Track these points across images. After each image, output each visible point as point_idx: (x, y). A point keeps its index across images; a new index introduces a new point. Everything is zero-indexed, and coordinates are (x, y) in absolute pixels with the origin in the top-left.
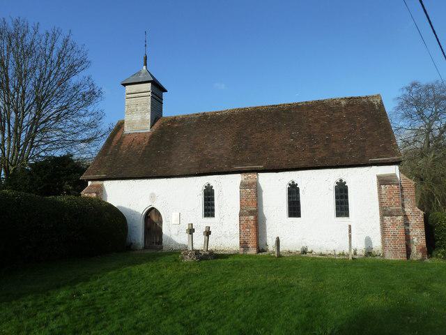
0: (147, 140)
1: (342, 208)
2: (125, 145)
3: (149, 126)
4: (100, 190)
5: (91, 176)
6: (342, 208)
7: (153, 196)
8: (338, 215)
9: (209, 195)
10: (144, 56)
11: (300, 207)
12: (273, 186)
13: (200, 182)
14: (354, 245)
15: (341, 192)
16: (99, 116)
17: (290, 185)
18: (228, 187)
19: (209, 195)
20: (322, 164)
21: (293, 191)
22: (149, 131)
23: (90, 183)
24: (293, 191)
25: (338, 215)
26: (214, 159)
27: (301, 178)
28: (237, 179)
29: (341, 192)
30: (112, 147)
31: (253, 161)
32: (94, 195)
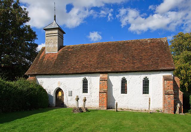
1: (146, 90)
6: (146, 90)
7: (59, 83)
8: (144, 93)
12: (116, 80)
14: (151, 109)
15: (146, 83)
18: (94, 81)
20: (138, 70)
21: (124, 82)
24: (124, 82)
25: (144, 93)
29: (146, 83)
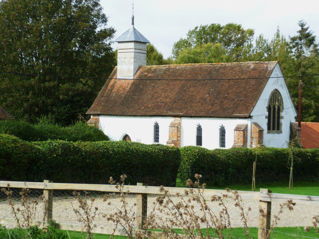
0: (129, 86)
2: (115, 90)
3: (132, 75)
4: (97, 122)
5: (92, 113)
9: (157, 127)
10: (132, 16)
11: (202, 140)
13: (151, 121)
16: (86, 111)
17: (198, 125)
19: (157, 127)
21: (199, 129)
22: (132, 78)
23: (92, 117)
26: (161, 105)
27: (159, 120)
28: (171, 120)
30: (107, 91)
31: (180, 110)
32: (93, 125)
